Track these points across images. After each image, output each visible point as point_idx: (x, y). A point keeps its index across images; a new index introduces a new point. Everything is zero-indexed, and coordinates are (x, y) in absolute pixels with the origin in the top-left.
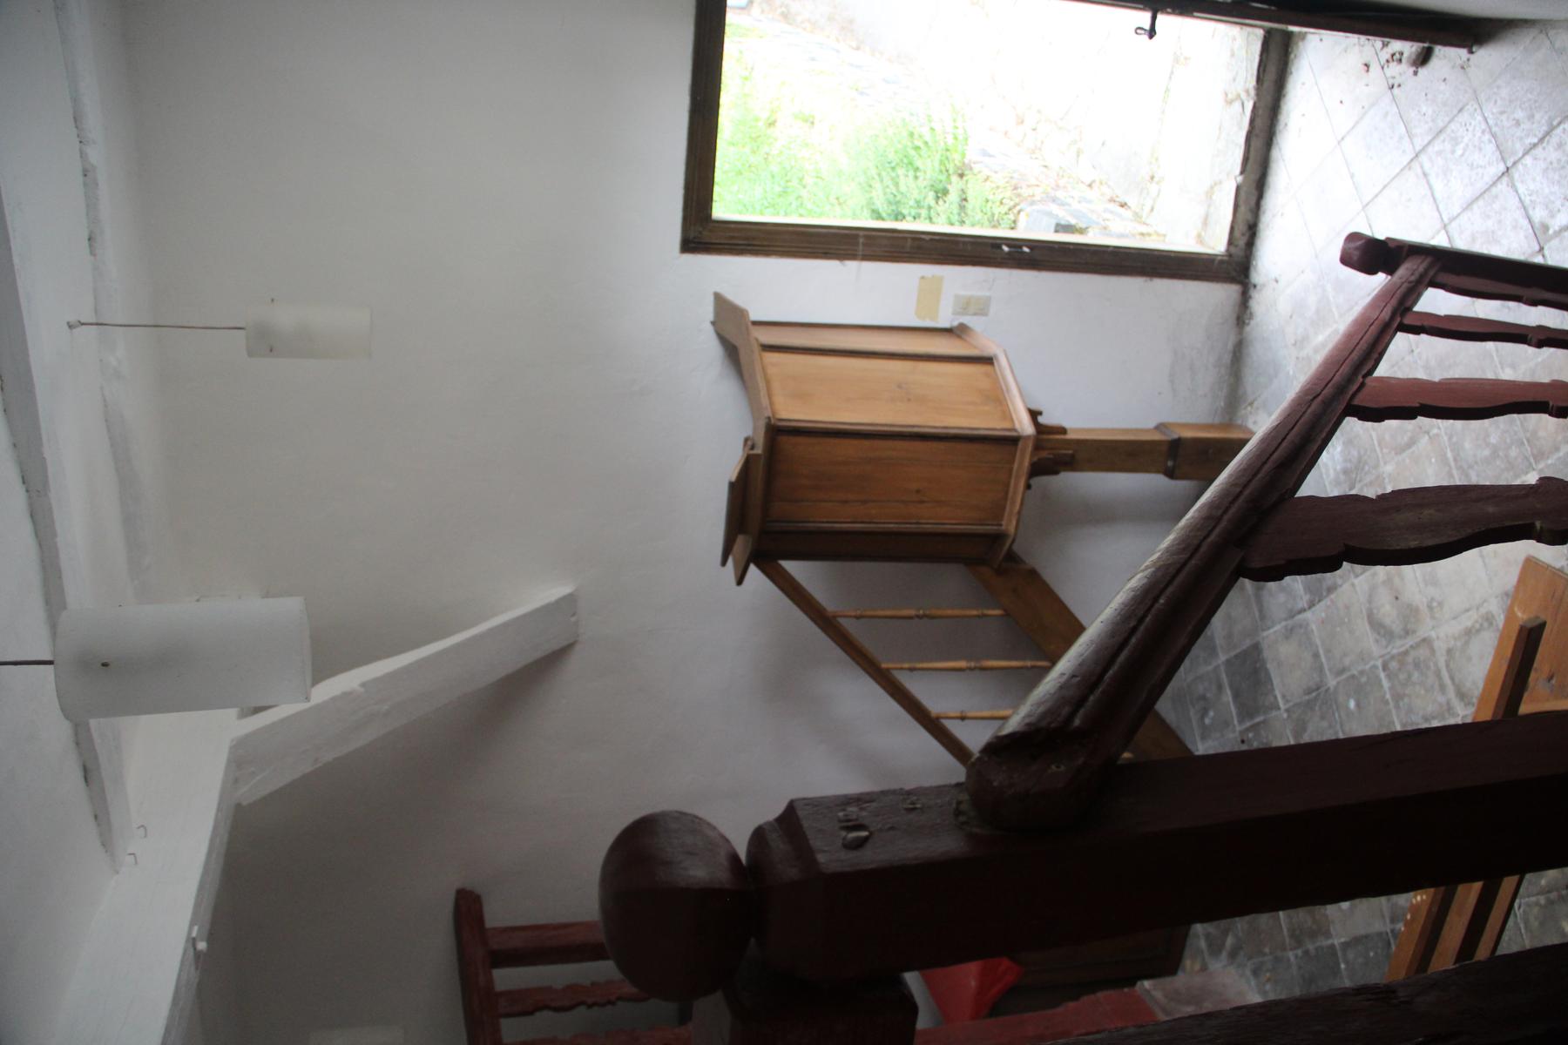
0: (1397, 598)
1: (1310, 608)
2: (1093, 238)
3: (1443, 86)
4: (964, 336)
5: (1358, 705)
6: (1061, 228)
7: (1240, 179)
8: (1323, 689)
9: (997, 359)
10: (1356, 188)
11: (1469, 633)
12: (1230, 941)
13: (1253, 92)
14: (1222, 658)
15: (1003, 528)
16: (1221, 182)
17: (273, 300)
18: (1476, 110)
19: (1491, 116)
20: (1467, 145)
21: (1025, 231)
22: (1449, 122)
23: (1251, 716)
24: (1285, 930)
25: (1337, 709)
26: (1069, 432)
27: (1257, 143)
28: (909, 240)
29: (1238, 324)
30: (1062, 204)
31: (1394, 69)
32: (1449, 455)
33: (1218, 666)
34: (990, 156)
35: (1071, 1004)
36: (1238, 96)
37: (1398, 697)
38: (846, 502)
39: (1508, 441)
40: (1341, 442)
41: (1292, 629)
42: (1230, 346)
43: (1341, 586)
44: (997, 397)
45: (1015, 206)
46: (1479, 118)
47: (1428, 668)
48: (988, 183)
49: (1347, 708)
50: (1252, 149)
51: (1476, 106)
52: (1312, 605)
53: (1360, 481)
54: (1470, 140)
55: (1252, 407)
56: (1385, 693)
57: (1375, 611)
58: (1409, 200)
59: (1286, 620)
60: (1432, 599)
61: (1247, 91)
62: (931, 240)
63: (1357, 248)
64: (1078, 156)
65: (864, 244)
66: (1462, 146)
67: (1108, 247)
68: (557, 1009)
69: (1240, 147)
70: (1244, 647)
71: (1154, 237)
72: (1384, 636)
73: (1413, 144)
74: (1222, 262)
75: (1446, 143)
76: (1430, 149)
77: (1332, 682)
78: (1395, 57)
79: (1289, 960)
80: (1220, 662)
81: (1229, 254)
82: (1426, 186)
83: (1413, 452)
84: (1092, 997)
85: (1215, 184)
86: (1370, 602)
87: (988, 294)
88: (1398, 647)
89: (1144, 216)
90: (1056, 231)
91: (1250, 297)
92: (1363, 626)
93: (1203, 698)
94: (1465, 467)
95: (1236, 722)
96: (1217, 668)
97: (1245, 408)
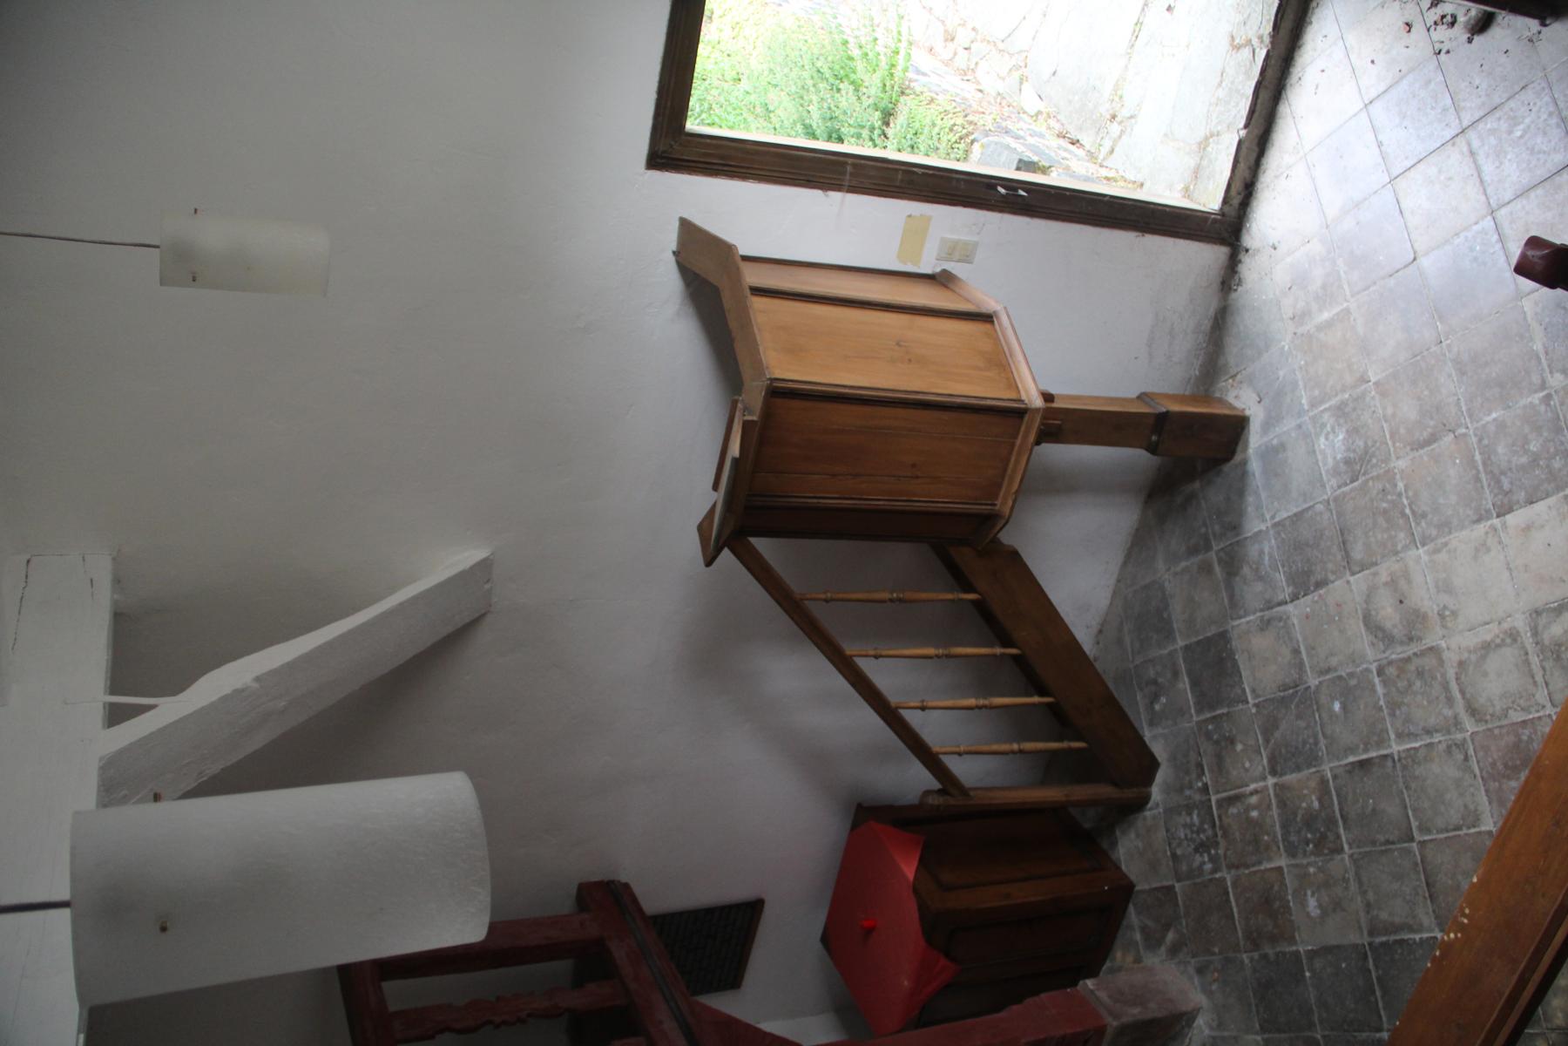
0: (1401, 602)
1: (1292, 601)
2: (1054, 179)
3: (1503, 59)
4: (950, 285)
5: (1344, 707)
6: (1024, 165)
7: (1243, 133)
8: (1302, 687)
9: (997, 318)
10: (1383, 158)
11: (1487, 647)
12: (1170, 936)
13: (1267, 40)
14: (1181, 643)
15: (997, 508)
16: (1218, 134)
17: (196, 211)
18: (1543, 88)
19: (1562, 98)
20: (1529, 127)
21: (976, 164)
22: (1508, 99)
23: (1212, 708)
24: (1240, 934)
25: (1318, 710)
26: (1055, 400)
27: (1264, 95)
28: (900, 172)
29: (1222, 290)
30: (1017, 138)
31: (1442, 33)
32: (1478, 457)
33: (1176, 650)
34: (924, 74)
35: (1015, 1007)
36: (1249, 42)
37: (1394, 706)
38: (834, 475)
39: (1552, 450)
40: (1344, 430)
41: (1269, 621)
42: (1212, 312)
43: (1333, 582)
44: (999, 362)
45: (967, 135)
46: (1547, 99)
47: (1434, 678)
48: (933, 106)
49: (1331, 710)
50: (1259, 101)
51: (1544, 84)
52: (1295, 598)
53: (1364, 474)
54: (1532, 122)
55: (1234, 380)
56: (1379, 699)
57: (1373, 613)
58: (1450, 179)
59: (1262, 610)
60: (1445, 607)
61: (1261, 38)
62: (923, 173)
63: (1542, 257)
64: (1021, 83)
65: (851, 174)
66: (1522, 127)
67: (1105, 196)
68: (460, 1032)
69: (1247, 98)
70: (1209, 634)
71: (1121, 183)
72: (1383, 640)
73: (1459, 118)
74: (1215, 221)
75: (1502, 122)
76: (1481, 126)
77: (1313, 682)
78: (1445, 20)
79: (1242, 962)
80: (1178, 647)
81: (1222, 212)
82: (1472, 165)
83: (1433, 450)
84: (1036, 998)
85: (1212, 136)
86: (1367, 602)
87: (975, 239)
88: (1397, 653)
89: (1101, 157)
90: (1018, 169)
91: (1240, 261)
92: (1356, 627)
93: (1155, 682)
94: (1496, 471)
95: (1193, 711)
96: (1171, 654)
97: (1227, 380)
